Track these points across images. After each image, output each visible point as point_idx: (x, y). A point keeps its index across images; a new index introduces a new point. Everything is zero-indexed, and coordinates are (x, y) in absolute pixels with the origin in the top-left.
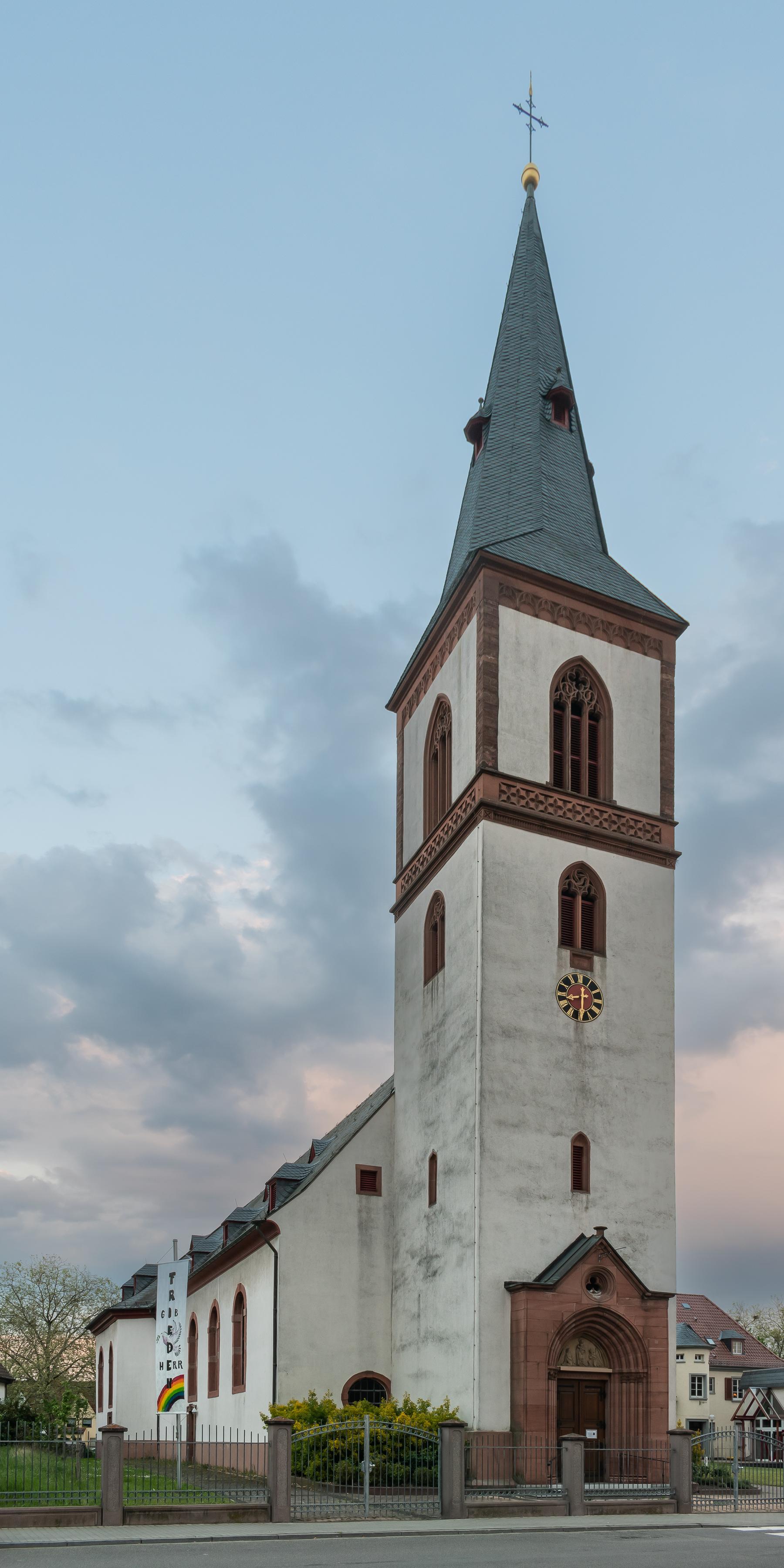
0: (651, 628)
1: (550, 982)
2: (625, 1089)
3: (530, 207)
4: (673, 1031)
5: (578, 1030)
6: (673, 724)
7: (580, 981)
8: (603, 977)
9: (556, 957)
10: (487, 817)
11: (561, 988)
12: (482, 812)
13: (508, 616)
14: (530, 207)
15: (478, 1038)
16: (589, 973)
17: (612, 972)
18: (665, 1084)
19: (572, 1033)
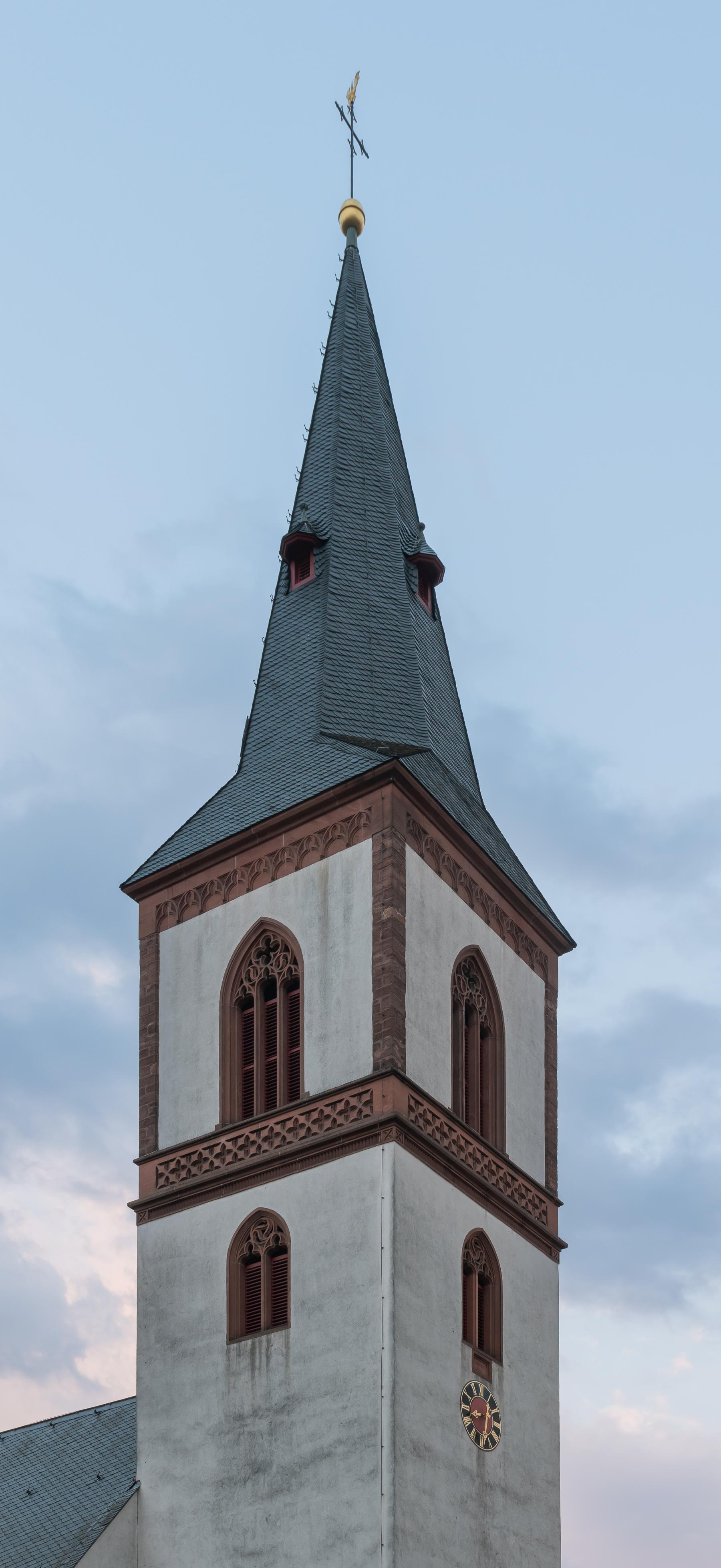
1: (455, 1390)
2: (521, 1549)
5: (481, 1460)
6: (556, 1069)
7: (482, 1393)
8: (501, 1392)
9: (460, 1355)
10: (397, 1139)
15: (386, 1451)
16: (488, 1383)
17: (510, 1380)
19: (475, 1464)
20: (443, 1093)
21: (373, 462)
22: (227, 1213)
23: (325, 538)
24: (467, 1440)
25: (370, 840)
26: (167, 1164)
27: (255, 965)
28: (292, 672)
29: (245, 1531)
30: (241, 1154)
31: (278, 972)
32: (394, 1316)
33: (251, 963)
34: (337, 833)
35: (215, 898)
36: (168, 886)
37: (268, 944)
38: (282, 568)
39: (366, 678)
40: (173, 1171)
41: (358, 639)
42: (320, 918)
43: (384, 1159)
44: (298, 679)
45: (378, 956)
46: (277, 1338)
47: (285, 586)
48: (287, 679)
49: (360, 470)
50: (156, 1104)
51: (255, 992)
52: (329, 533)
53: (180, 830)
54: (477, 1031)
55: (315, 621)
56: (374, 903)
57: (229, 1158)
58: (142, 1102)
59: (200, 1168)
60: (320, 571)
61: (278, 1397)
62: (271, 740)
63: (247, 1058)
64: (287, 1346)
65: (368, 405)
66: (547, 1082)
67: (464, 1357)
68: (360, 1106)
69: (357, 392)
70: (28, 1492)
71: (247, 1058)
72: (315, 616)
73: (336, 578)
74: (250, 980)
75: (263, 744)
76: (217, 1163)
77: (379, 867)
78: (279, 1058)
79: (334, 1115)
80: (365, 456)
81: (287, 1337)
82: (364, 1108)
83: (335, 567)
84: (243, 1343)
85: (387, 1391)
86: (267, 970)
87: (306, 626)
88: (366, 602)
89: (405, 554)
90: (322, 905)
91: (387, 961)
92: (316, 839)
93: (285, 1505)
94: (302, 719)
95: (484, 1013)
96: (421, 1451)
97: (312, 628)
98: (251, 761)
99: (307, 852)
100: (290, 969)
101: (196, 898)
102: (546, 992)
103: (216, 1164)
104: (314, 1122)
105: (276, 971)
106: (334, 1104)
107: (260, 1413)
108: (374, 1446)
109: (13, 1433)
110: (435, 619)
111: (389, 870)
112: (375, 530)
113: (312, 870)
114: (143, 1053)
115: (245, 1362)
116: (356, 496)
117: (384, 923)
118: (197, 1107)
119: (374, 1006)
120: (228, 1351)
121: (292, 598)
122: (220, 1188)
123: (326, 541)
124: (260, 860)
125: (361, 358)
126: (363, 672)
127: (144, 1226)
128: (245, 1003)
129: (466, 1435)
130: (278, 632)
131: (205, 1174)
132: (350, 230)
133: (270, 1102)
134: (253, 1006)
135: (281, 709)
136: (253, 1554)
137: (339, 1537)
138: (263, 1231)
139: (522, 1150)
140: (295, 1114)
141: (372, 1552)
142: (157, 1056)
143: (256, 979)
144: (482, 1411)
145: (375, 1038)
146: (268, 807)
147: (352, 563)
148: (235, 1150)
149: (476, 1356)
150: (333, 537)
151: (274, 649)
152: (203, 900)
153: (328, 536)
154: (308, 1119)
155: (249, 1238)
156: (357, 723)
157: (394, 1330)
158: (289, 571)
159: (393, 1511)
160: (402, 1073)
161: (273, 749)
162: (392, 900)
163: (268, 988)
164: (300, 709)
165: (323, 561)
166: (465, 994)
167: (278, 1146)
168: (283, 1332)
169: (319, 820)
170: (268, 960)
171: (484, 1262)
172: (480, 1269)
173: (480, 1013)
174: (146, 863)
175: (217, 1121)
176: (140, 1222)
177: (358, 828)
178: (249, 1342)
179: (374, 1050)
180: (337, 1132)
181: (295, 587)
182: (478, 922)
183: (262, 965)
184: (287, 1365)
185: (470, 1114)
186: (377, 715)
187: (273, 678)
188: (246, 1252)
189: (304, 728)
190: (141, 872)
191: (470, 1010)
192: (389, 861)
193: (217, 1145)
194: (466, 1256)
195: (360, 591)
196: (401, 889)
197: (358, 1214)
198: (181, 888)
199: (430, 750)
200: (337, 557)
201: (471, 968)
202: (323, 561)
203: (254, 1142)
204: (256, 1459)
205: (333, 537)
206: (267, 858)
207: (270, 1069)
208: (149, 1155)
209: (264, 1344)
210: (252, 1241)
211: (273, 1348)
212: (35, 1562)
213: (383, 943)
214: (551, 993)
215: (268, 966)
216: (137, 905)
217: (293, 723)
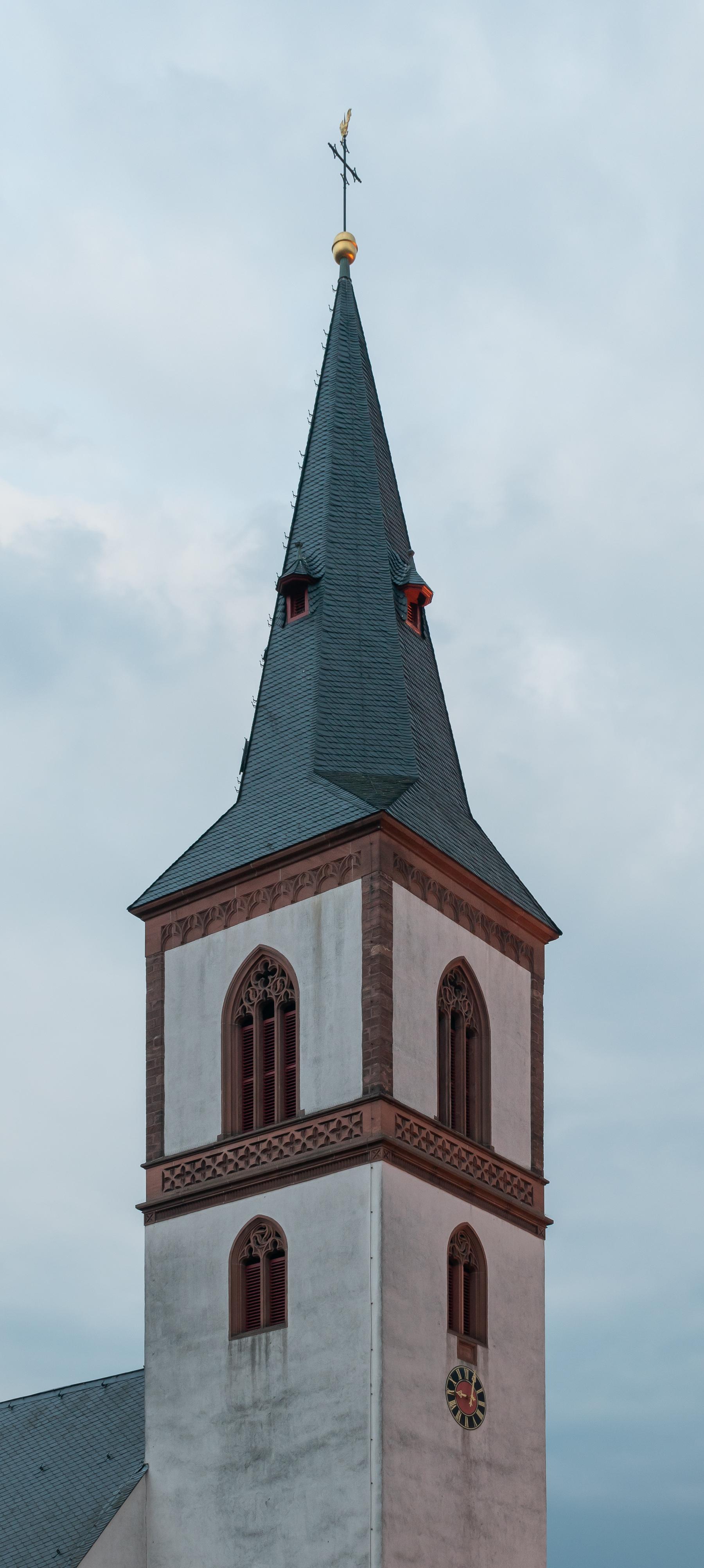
0: (521, 927)
1: (441, 1377)
2: (505, 1516)
3: (345, 291)
4: (545, 1446)
5: (465, 1439)
8: (486, 1373)
10: (385, 1158)
11: (450, 1386)
12: (382, 1150)
13: (400, 894)
14: (345, 291)
15: (375, 1445)
16: (473, 1366)
17: (495, 1367)
18: (539, 1512)
19: (460, 1443)
20: (427, 1104)
21: (365, 496)
22: (228, 1219)
23: (319, 575)
24: (452, 1424)
25: (360, 881)
26: (172, 1169)
27: (254, 987)
28: (288, 706)
29: (247, 1514)
30: (242, 1164)
31: (277, 997)
32: (382, 1321)
33: (250, 985)
34: (330, 872)
35: (217, 923)
36: (173, 909)
37: (265, 967)
38: (278, 600)
39: (357, 713)
40: (178, 1176)
41: (349, 674)
42: (314, 949)
43: (370, 1177)
44: (293, 714)
45: (367, 989)
46: (275, 1336)
47: (280, 620)
48: (284, 713)
49: (352, 505)
50: (162, 1113)
51: (254, 1012)
52: (323, 571)
53: (183, 856)
54: (463, 1033)
55: (310, 657)
56: (363, 940)
57: (231, 1167)
58: (148, 1110)
59: (204, 1175)
60: (314, 608)
61: (277, 1390)
62: (269, 772)
63: (247, 1071)
64: (285, 1344)
65: (360, 438)
66: (533, 1069)
67: (449, 1346)
68: (351, 1126)
69: (350, 426)
70: (41, 1468)
71: (247, 1071)
72: (309, 653)
73: (329, 616)
74: (250, 1001)
75: (261, 775)
76: (219, 1171)
77: (369, 906)
78: (277, 1072)
79: (327, 1133)
80: (357, 490)
81: (285, 1336)
82: (354, 1128)
83: (328, 605)
84: (244, 1339)
85: (375, 1389)
86: (265, 993)
87: (301, 662)
88: (357, 637)
89: (394, 584)
90: (317, 935)
91: (375, 995)
92: (310, 877)
93: (283, 1490)
94: (298, 754)
95: (470, 1016)
96: (407, 1440)
97: (306, 664)
98: (249, 790)
99: (302, 887)
100: (286, 994)
101: (199, 922)
102: (532, 982)
103: (218, 1173)
104: (309, 1138)
105: (274, 994)
106: (327, 1123)
107: (260, 1405)
108: (364, 1438)
109: (22, 1402)
110: (423, 637)
111: (377, 911)
112: (367, 564)
113: (306, 904)
114: (149, 1064)
115: (246, 1357)
116: (348, 531)
117: (372, 959)
118: (201, 1119)
119: (363, 1035)
120: (230, 1347)
121: (288, 631)
122: (222, 1194)
123: (319, 579)
124: (259, 891)
125: (354, 391)
126: (355, 707)
127: (151, 1227)
128: (246, 1020)
129: (451, 1418)
130: (275, 664)
131: (209, 1181)
132: (343, 261)
133: (268, 1118)
134: (252, 1023)
135: (278, 741)
136: (253, 1535)
137: (332, 1521)
138: (263, 1235)
139: (508, 1142)
140: (292, 1130)
141: (363, 1535)
142: (163, 1067)
143: (255, 1000)
144: (468, 1392)
145: (365, 1065)
146: (266, 844)
147: (344, 599)
148: (236, 1160)
149: (461, 1343)
150: (327, 575)
151: (271, 681)
152: (205, 925)
153: (321, 573)
154: (303, 1135)
155: (249, 1242)
156: (349, 758)
157: (382, 1333)
158: (285, 604)
159: (382, 1498)
160: (389, 1097)
161: (271, 781)
162: (380, 938)
163: (266, 1008)
164: (296, 744)
165: (317, 598)
166: (451, 1003)
167: (276, 1159)
168: (281, 1331)
169: (314, 859)
170: (266, 983)
171: (469, 1252)
172: (466, 1260)
173: (466, 1017)
174: (152, 886)
175: (219, 1131)
176: (147, 1222)
177: (349, 869)
178: (250, 1339)
179: (364, 1076)
180: (330, 1149)
181: (290, 620)
182: (464, 934)
183: (261, 988)
184: (285, 1362)
185: (457, 1113)
186: (367, 748)
187: (270, 710)
188: (246, 1254)
189: (299, 764)
190: (147, 895)
191: (456, 1016)
192: (377, 902)
193: (220, 1154)
194: (452, 1250)
195: (352, 626)
196: (389, 926)
197: (349, 1225)
198: (185, 912)
199: (417, 780)
200: (330, 595)
201: (458, 980)
202: (317, 598)
203: (253, 1154)
204: (256, 1447)
205: (327, 575)
206: (265, 890)
207: (268, 1083)
208: (155, 1159)
209: (264, 1341)
210: (252, 1244)
211: (271, 1345)
212: (51, 1543)
213: (371, 977)
214: (538, 983)
215: (266, 989)
216: (144, 923)
217: (289, 758)
